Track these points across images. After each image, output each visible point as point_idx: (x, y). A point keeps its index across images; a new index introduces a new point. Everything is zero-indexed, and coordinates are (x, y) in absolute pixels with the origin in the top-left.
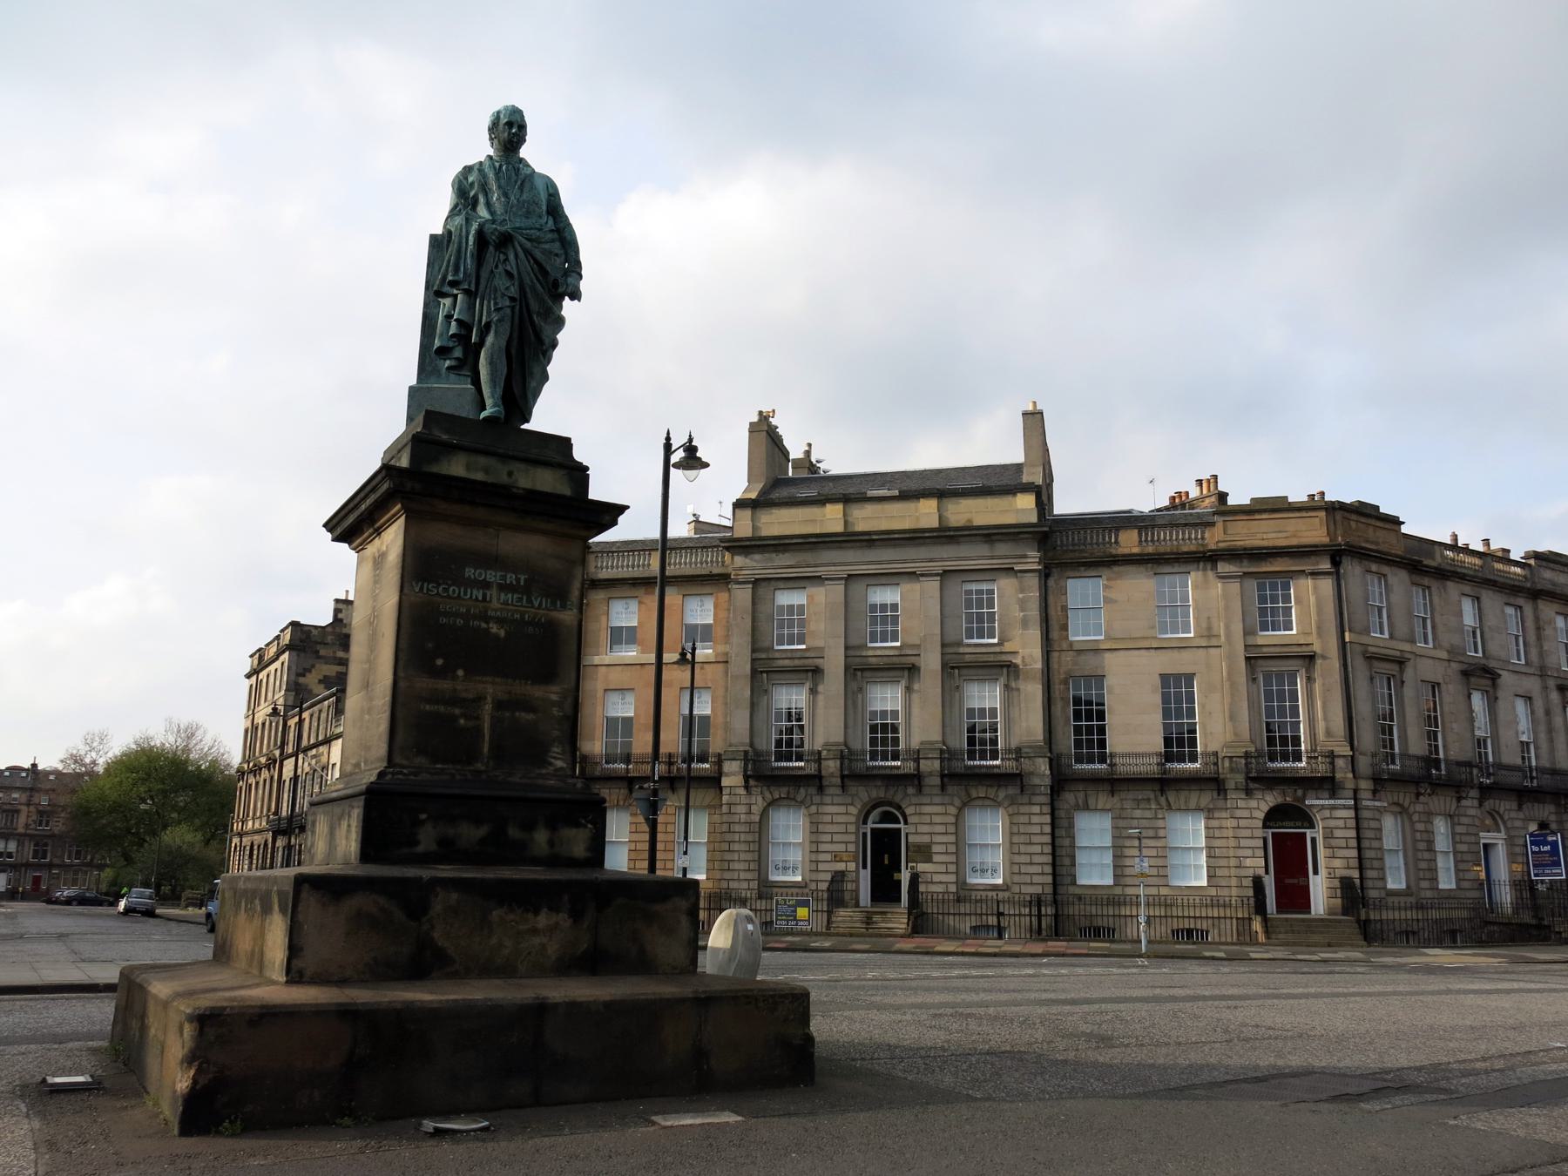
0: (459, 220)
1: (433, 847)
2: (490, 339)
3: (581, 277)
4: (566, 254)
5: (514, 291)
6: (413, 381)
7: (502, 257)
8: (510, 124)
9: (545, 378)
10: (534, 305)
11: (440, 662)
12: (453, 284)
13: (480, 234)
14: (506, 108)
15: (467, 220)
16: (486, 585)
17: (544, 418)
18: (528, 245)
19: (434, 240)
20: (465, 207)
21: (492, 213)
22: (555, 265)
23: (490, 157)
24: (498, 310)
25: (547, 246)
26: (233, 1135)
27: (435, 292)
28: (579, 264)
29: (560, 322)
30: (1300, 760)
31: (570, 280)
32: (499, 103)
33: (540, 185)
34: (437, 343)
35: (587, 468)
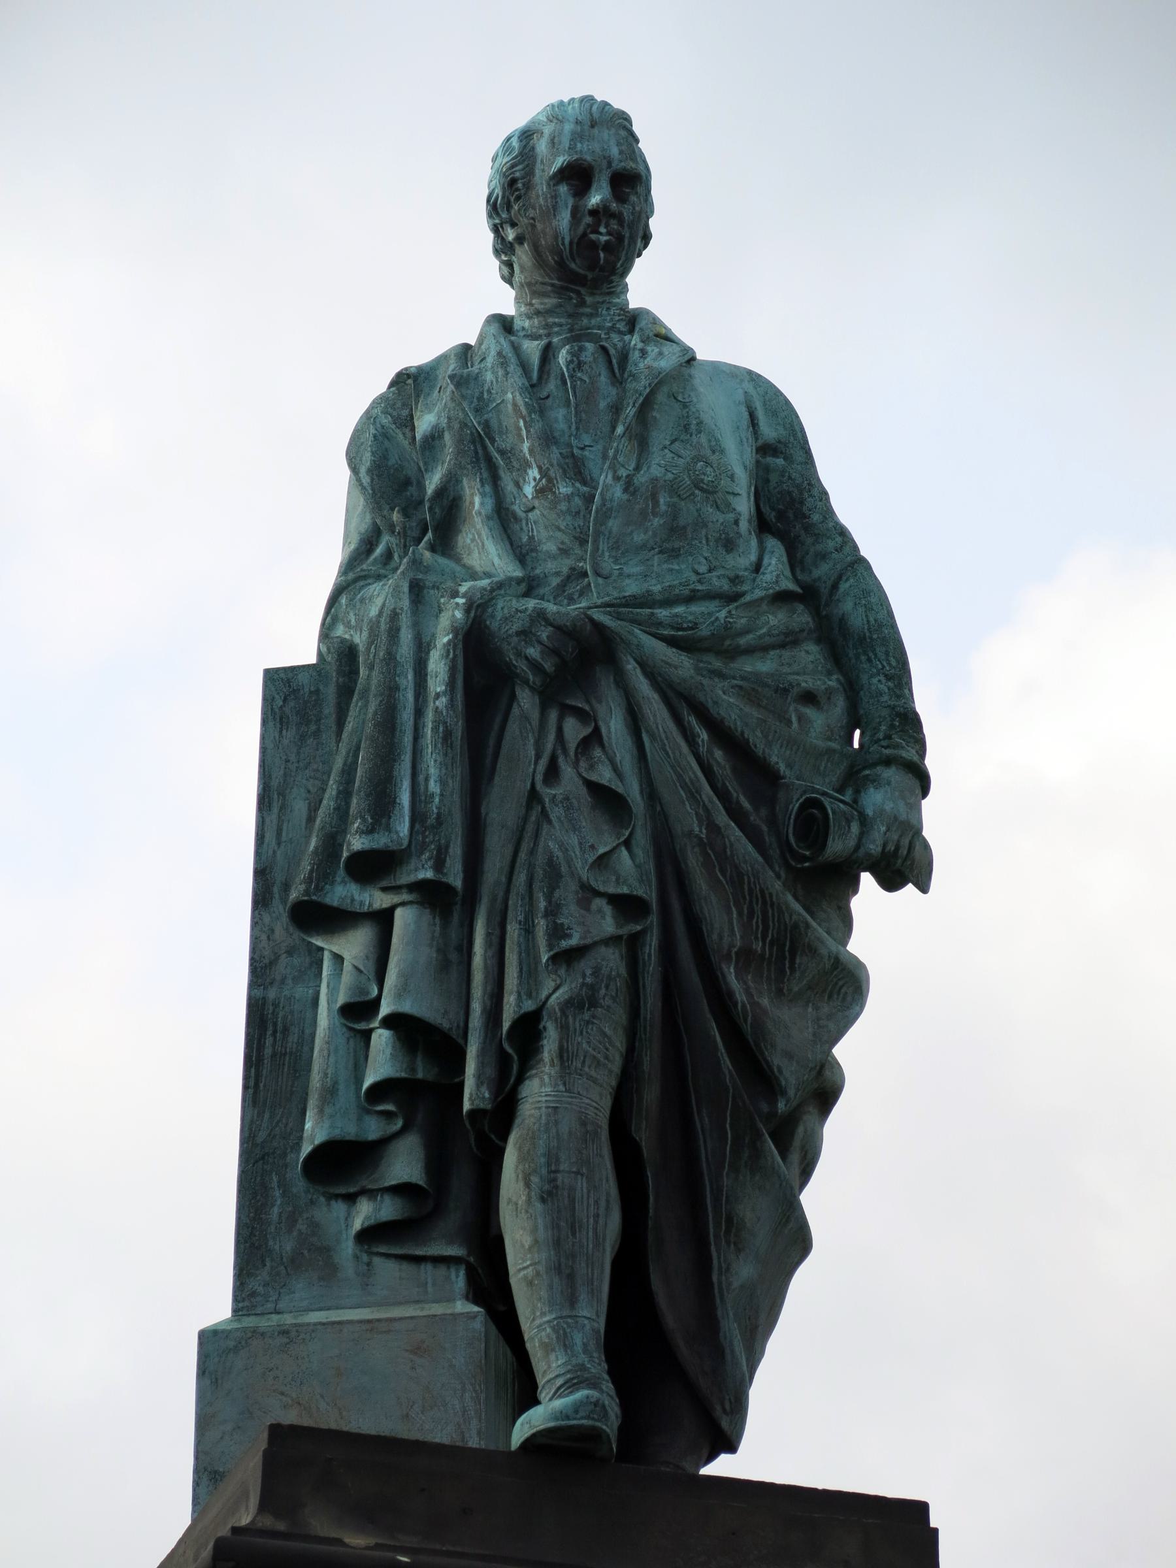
0: (379, 597)
2: (538, 1092)
3: (923, 782)
4: (852, 690)
5: (631, 871)
6: (218, 1306)
7: (574, 731)
8: (577, 176)
9: (795, 1241)
12: (372, 867)
13: (477, 646)
14: (556, 113)
15: (417, 590)
17: (800, 1423)
18: (682, 666)
19: (285, 693)
20: (410, 539)
21: (522, 553)
22: (807, 743)
23: (504, 324)
24: (567, 958)
25: (764, 666)
26: (667, 338)
27: (294, 909)
28: (909, 725)
29: (845, 988)
31: (874, 799)
32: (526, 95)
33: (720, 413)
34: (315, 1131)
35: (920, 1509)
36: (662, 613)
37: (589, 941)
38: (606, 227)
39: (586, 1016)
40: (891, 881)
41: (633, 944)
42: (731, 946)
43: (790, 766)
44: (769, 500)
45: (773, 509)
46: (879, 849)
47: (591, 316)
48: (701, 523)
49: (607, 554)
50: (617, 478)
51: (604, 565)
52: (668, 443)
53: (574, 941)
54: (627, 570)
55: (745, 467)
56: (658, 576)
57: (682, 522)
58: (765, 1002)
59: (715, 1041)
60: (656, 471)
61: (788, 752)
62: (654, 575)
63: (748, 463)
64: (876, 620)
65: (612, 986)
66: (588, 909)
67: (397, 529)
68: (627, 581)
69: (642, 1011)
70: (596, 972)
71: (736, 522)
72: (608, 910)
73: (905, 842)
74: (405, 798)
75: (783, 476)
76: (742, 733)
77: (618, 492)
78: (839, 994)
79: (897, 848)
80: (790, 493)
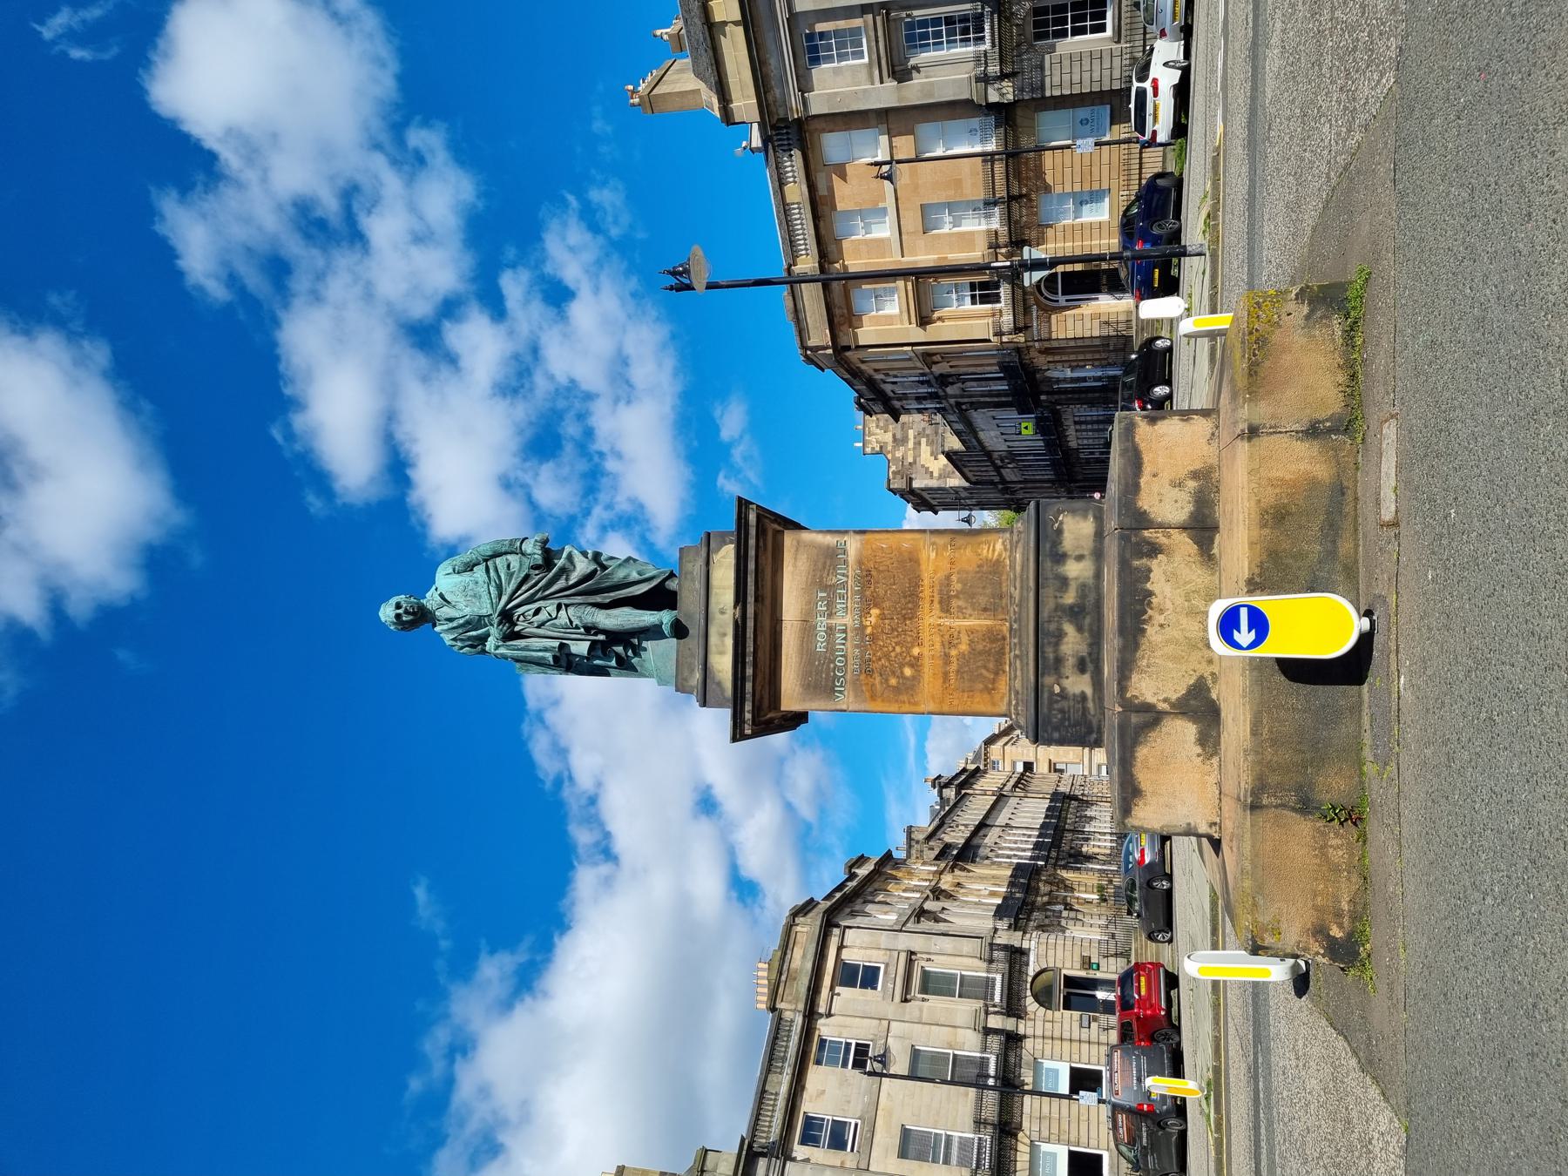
1: (1087, 677)
10: (561, 584)
11: (908, 672)
16: (830, 630)
18: (504, 599)
30: (994, 980)
41: (567, 606)
76: (84, 21)
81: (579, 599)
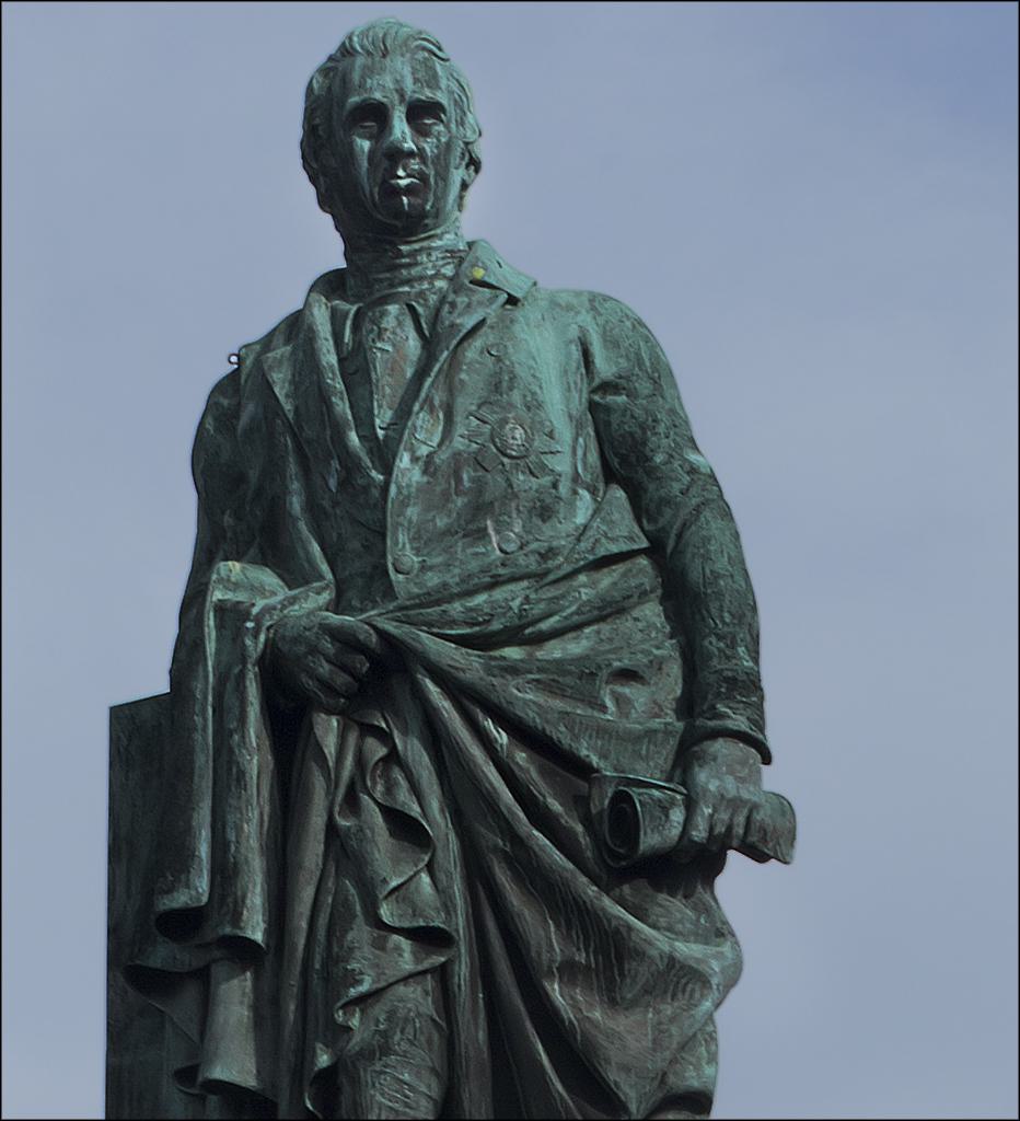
10: (546, 938)
18: (468, 664)
36: (456, 608)
37: (383, 984)
38: (405, 171)
39: (378, 1067)
40: (760, 857)
41: (443, 974)
42: (552, 961)
43: (604, 756)
44: (612, 444)
45: (616, 455)
46: (704, 835)
47: (409, 266)
48: (511, 493)
49: (408, 546)
50: (415, 459)
51: (405, 559)
52: (474, 408)
53: (364, 988)
54: (430, 562)
55: (570, 417)
56: (462, 562)
57: (488, 497)
58: (597, 1015)
59: (542, 1066)
60: (459, 443)
61: (599, 743)
62: (457, 563)
63: (574, 413)
64: (711, 571)
65: (409, 1029)
66: (383, 948)
67: (229, 535)
68: (430, 574)
69: (457, 1050)
70: (391, 1015)
71: (555, 486)
72: (405, 944)
73: (741, 819)
74: (204, 850)
75: (624, 416)
76: (544, 729)
77: (416, 476)
78: (684, 991)
79: (730, 828)
80: (631, 434)
81: (475, 1034)
